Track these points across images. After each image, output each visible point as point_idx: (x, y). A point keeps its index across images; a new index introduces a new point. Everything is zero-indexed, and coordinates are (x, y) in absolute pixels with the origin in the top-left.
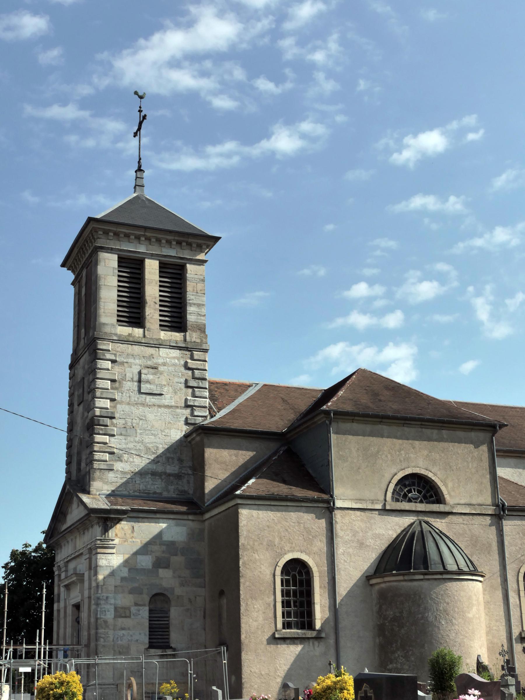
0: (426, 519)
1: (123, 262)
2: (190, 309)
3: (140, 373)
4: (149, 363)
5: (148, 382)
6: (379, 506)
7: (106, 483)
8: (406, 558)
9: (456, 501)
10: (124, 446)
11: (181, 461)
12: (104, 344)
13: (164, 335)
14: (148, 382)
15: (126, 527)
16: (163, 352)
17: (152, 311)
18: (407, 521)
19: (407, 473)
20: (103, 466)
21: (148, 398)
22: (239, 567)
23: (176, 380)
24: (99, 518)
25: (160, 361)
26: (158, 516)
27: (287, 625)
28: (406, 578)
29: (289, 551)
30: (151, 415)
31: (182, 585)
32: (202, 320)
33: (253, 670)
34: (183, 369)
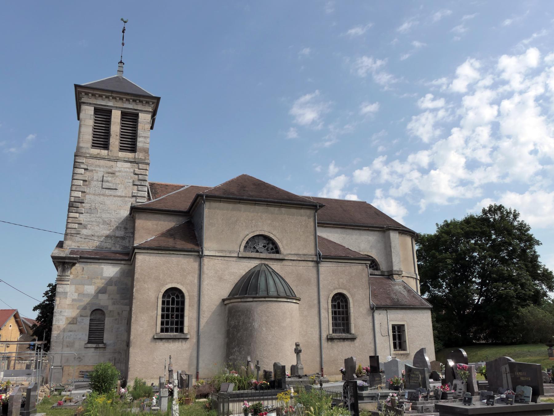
0: (266, 263)
1: (97, 111)
2: (139, 139)
3: (103, 176)
4: (110, 170)
5: (107, 181)
6: (236, 255)
7: (75, 242)
8: (248, 288)
9: (289, 252)
10: (89, 220)
11: (126, 229)
12: (80, 159)
13: (122, 154)
14: (107, 181)
15: (79, 268)
16: (119, 164)
17: (114, 140)
18: (252, 264)
19: (255, 234)
20: (73, 231)
21: (107, 191)
22: (133, 293)
23: (127, 180)
24: (59, 262)
25: (117, 169)
26: (101, 261)
27: (334, 331)
28: (242, 300)
29: (169, 283)
30: (108, 201)
31: (114, 304)
32: (147, 146)
33: (137, 359)
34: (132, 175)
